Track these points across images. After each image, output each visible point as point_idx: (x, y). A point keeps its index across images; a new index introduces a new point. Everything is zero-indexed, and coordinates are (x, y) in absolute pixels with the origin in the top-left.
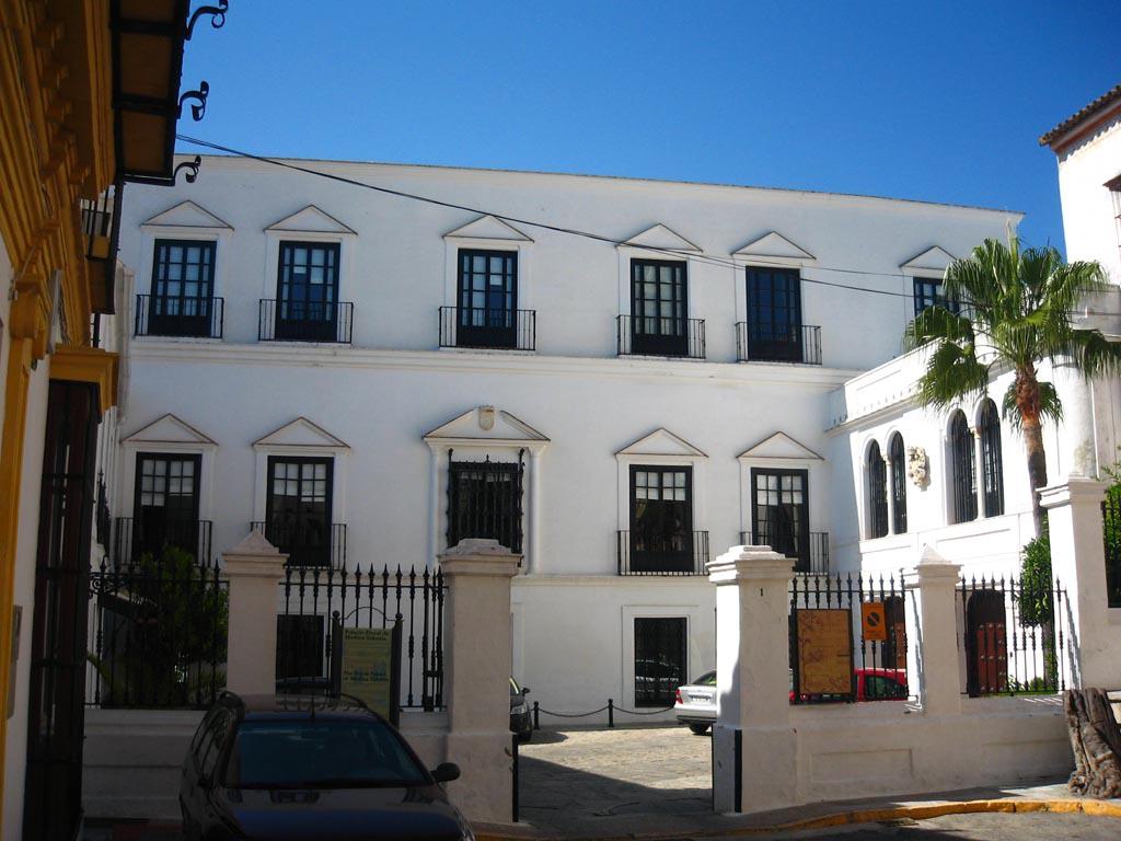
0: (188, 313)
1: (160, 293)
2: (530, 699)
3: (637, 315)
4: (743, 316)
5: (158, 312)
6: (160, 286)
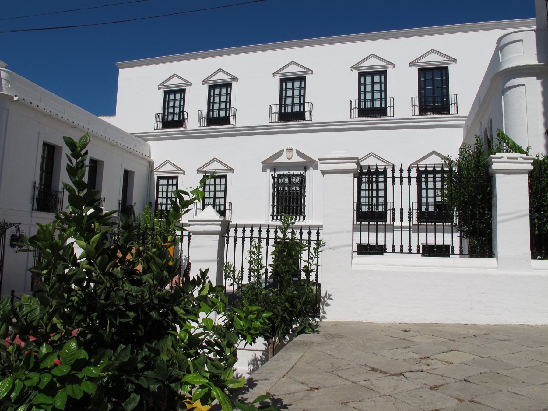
0: (222, 116)
1: (283, 103)
2: (329, 301)
3: (210, 110)
4: (416, 94)
5: (166, 120)
6: (362, 95)
